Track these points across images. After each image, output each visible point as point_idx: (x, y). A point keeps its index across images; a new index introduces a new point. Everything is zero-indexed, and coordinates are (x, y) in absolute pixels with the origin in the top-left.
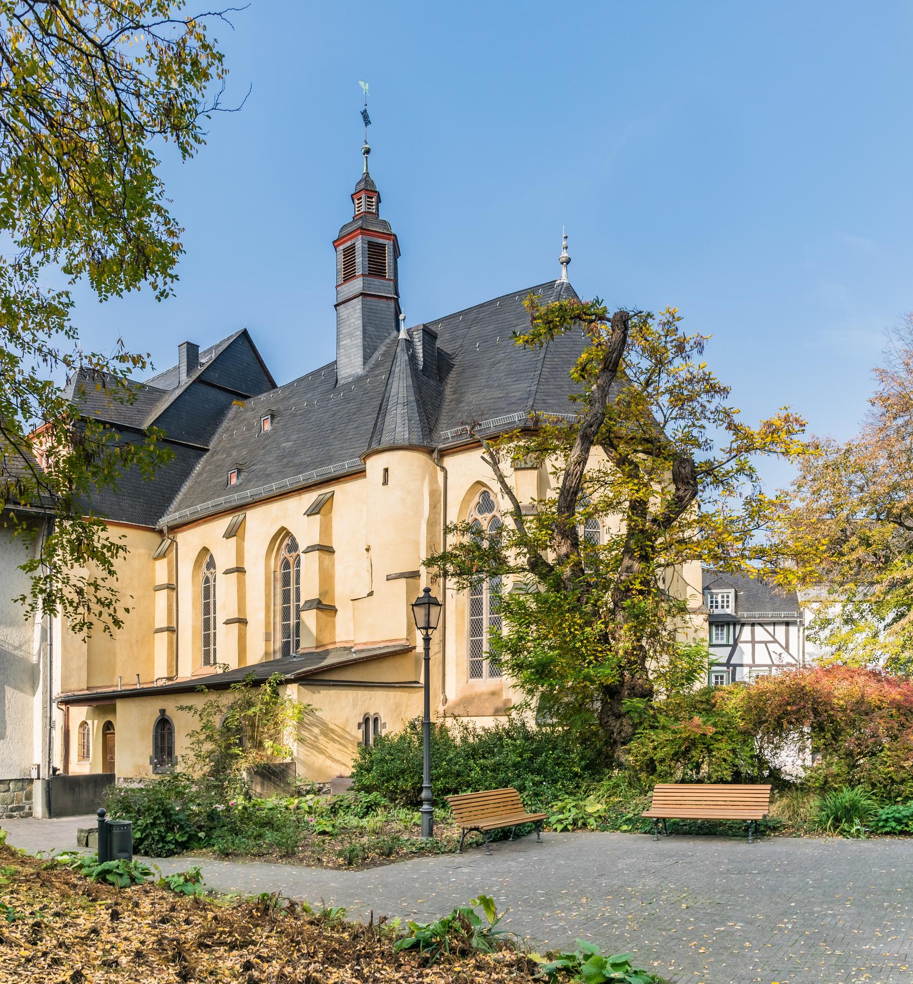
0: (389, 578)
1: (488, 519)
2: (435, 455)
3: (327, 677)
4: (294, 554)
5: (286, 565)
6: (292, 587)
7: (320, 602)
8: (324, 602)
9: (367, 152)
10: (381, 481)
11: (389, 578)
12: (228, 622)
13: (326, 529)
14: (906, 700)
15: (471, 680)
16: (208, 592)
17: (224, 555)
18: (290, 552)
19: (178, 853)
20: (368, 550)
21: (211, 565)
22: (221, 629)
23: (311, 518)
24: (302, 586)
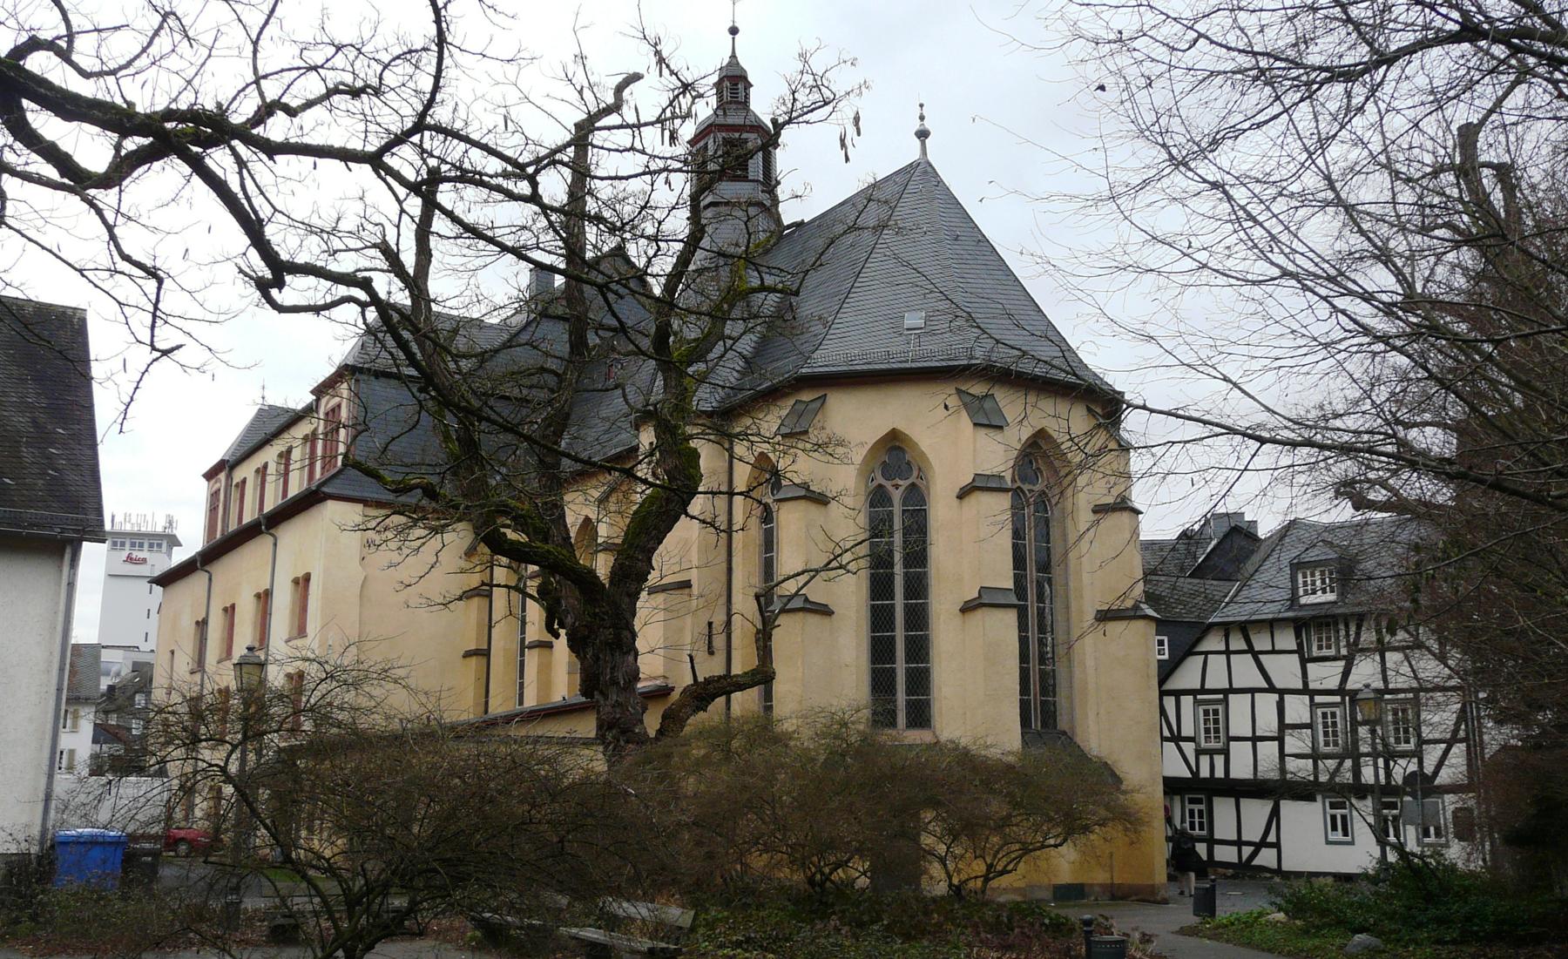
9: (734, 31)
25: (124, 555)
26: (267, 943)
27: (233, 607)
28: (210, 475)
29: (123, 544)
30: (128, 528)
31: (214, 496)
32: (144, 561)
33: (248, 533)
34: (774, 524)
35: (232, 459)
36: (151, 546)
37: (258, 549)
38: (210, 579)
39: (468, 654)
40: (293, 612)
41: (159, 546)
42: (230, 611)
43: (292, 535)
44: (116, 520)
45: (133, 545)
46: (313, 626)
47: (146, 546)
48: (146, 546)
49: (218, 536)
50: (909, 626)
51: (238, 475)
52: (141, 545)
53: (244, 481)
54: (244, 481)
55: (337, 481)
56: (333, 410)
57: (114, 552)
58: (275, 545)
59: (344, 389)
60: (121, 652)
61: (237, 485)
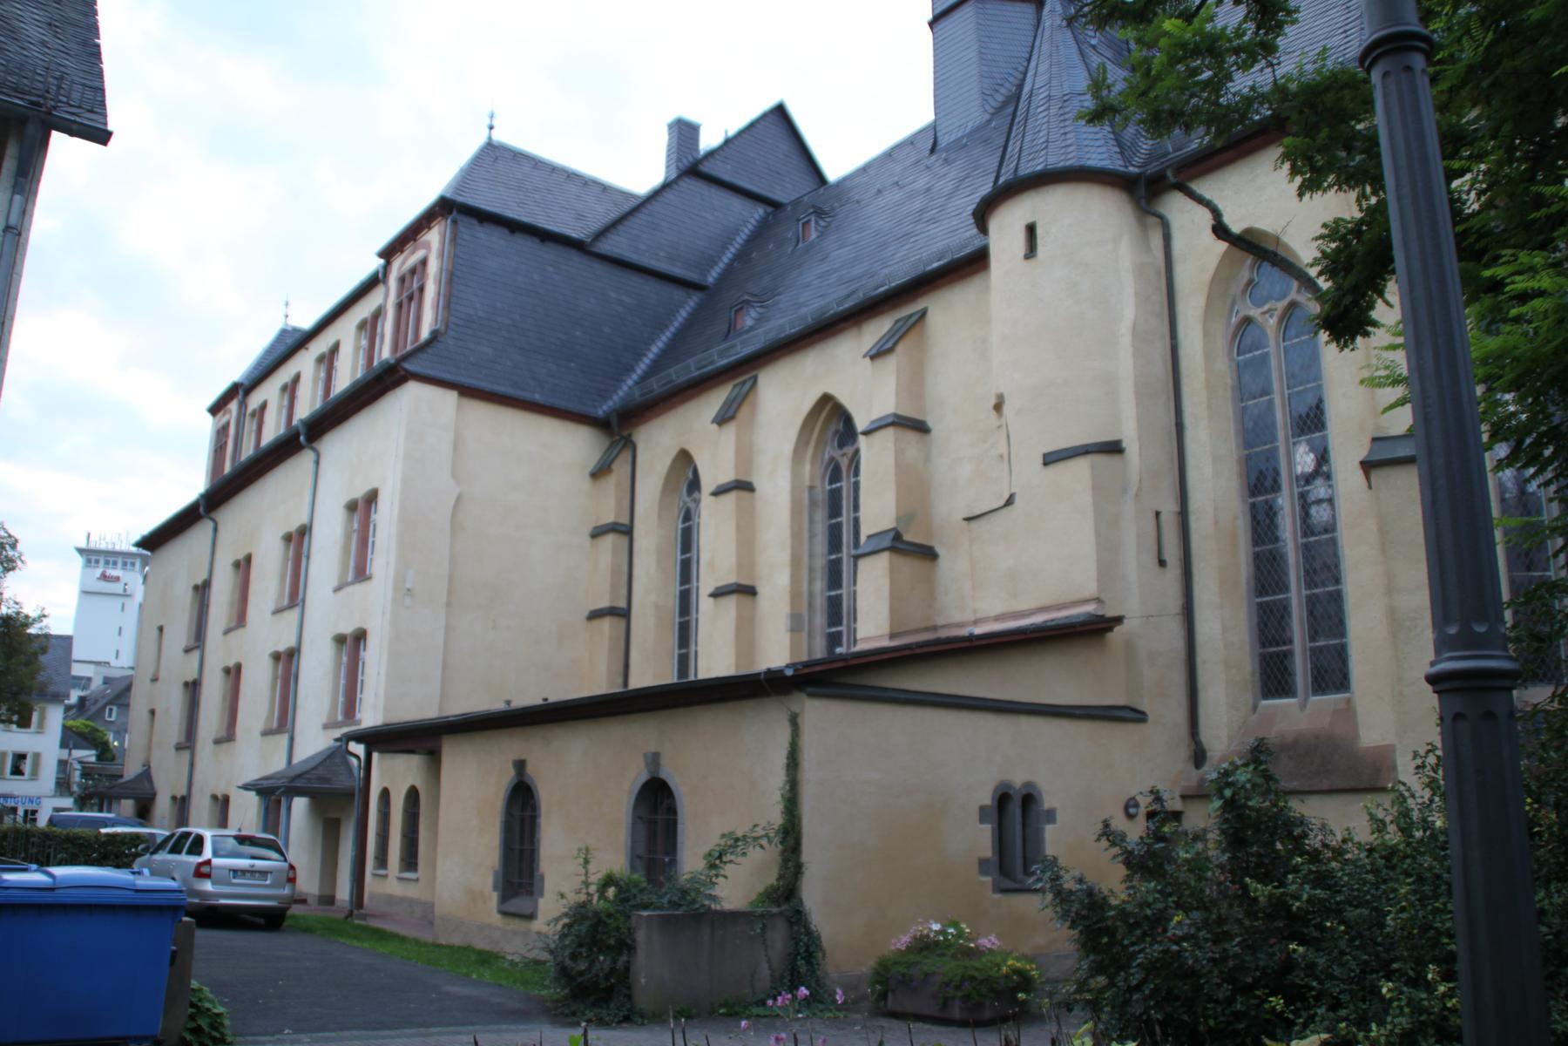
0: (1050, 459)
1: (1277, 314)
2: (1142, 191)
3: (912, 548)
4: (849, 450)
5: (835, 475)
6: (845, 519)
7: (897, 537)
8: (907, 537)
10: (1039, 231)
11: (1050, 459)
12: (718, 594)
13: (914, 382)
14: (795, 670)
15: (1314, 699)
16: (687, 540)
17: (715, 468)
18: (841, 445)
19: (1419, 9)
20: (998, 407)
21: (694, 485)
22: (705, 606)
23: (880, 362)
24: (862, 514)
25: (98, 572)
26: (54, 796)
27: (248, 559)
28: (215, 409)
29: (97, 562)
30: (103, 547)
31: (221, 433)
32: (117, 579)
33: (286, 448)
34: (828, 523)
35: (247, 383)
36: (125, 564)
37: (292, 475)
38: (216, 530)
39: (595, 615)
40: (346, 549)
41: (133, 564)
42: (244, 566)
43: (339, 446)
44: (92, 538)
45: (107, 563)
46: (383, 561)
47: (120, 564)
48: (120, 564)
49: (227, 469)
50: (1311, 577)
51: (254, 401)
52: (115, 563)
53: (264, 406)
54: (264, 406)
55: (423, 356)
56: (413, 271)
57: (88, 570)
58: (317, 463)
59: (434, 237)
60: (92, 667)
61: (253, 414)
